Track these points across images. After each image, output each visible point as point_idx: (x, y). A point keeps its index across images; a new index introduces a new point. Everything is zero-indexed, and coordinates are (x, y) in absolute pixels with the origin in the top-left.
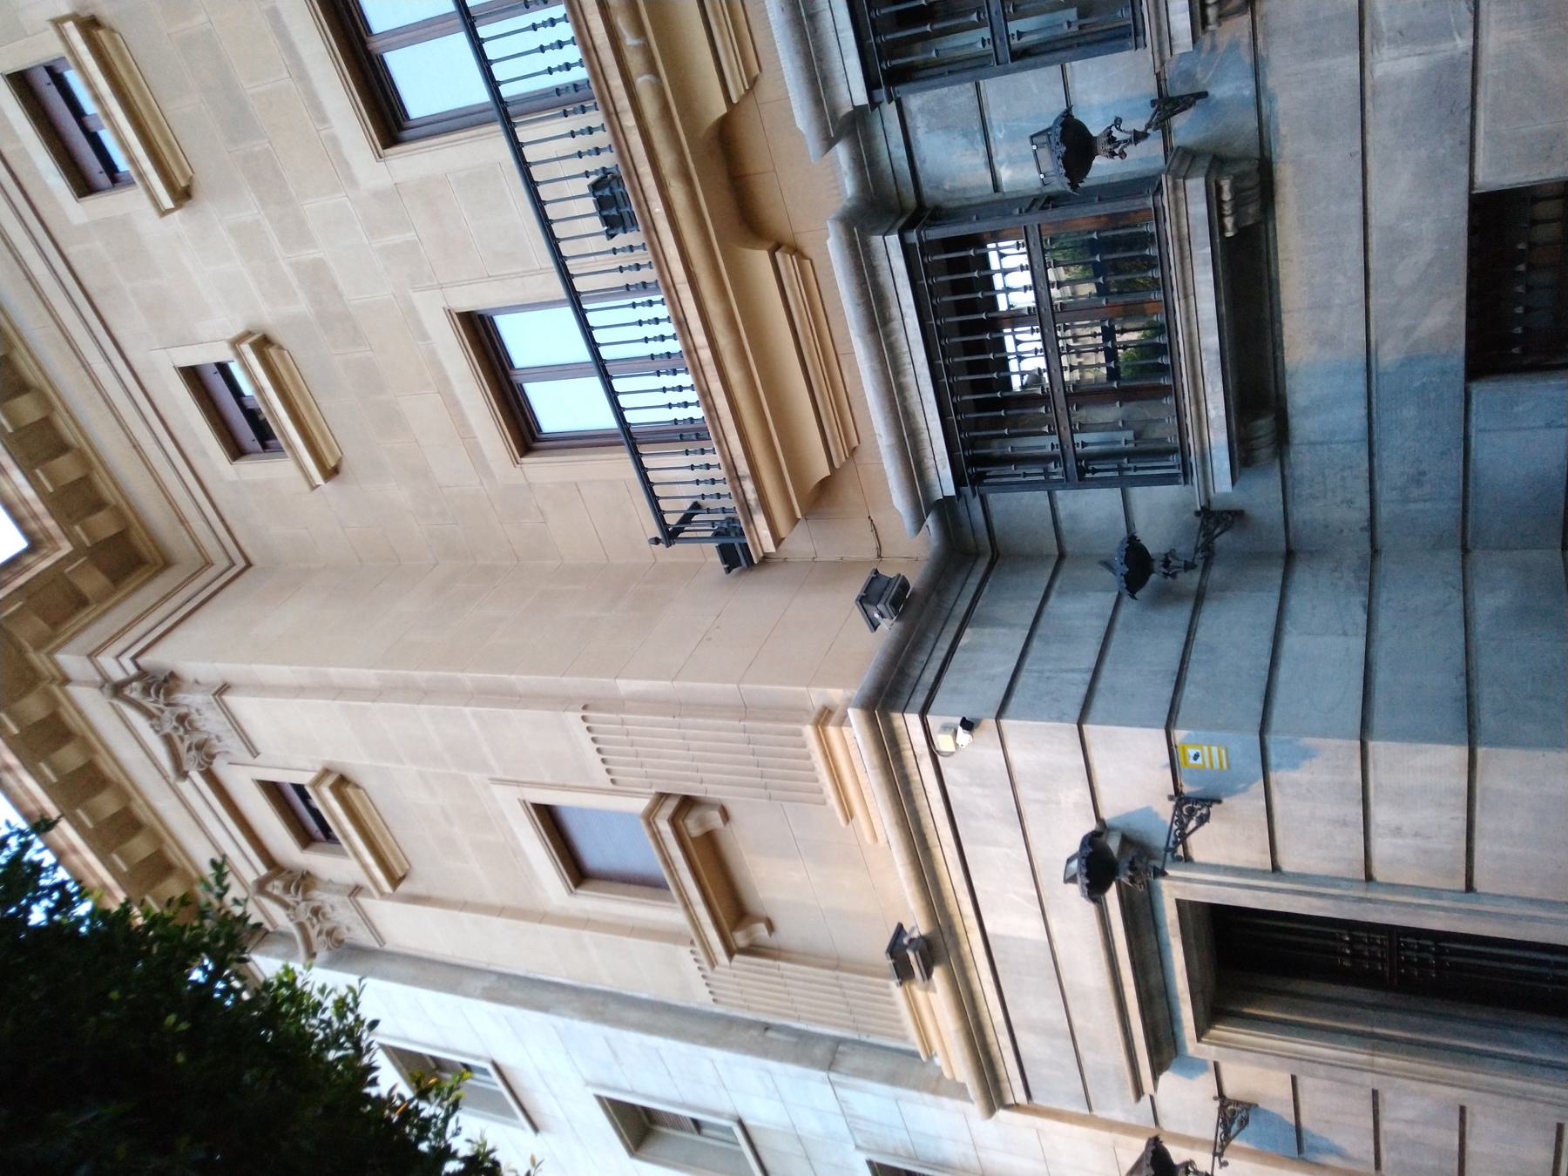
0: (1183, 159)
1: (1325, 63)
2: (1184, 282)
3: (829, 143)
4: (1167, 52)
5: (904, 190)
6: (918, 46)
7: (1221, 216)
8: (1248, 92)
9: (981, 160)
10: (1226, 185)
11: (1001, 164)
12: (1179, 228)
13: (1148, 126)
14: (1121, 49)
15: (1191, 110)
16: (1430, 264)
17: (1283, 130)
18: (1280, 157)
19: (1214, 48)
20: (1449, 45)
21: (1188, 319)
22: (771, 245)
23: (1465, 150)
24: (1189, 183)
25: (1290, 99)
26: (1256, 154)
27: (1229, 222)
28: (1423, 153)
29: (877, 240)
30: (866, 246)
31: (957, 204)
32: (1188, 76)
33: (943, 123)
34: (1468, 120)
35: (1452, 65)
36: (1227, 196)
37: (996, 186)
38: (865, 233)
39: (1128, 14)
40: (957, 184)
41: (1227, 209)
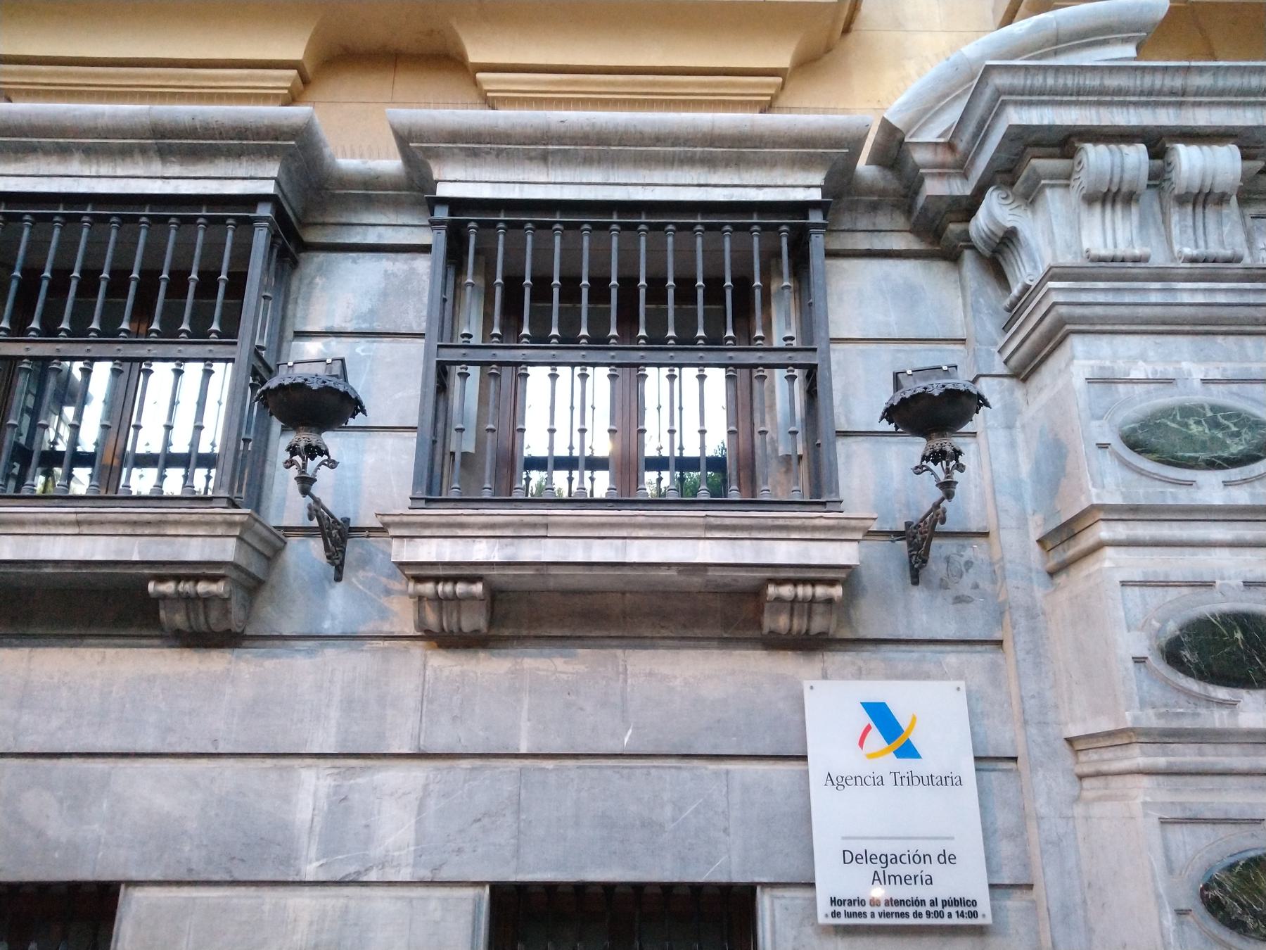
0: (270, 546)
1: (334, 714)
2: (102, 523)
3: (405, 139)
4: (398, 533)
5: (329, 230)
6: (481, 283)
7: (178, 579)
8: (327, 627)
9: (338, 324)
10: (218, 588)
11: (325, 345)
12: (176, 523)
13: (317, 501)
14: (416, 484)
15: (324, 560)
16: (40, 834)
17: (269, 664)
18: (238, 657)
19: (388, 592)
20: (313, 853)
21: (45, 523)
22: (309, 69)
23: (181, 875)
24: (232, 543)
25: (297, 671)
26: (250, 631)
27: (168, 588)
28: (192, 826)
29: (273, 169)
30: (268, 153)
31: (294, 288)
32: (364, 562)
33: (391, 292)
34: (216, 878)
35: (289, 859)
36: (202, 587)
37: (300, 335)
38: (286, 156)
39: (454, 494)
40: (317, 293)
41: (186, 587)
